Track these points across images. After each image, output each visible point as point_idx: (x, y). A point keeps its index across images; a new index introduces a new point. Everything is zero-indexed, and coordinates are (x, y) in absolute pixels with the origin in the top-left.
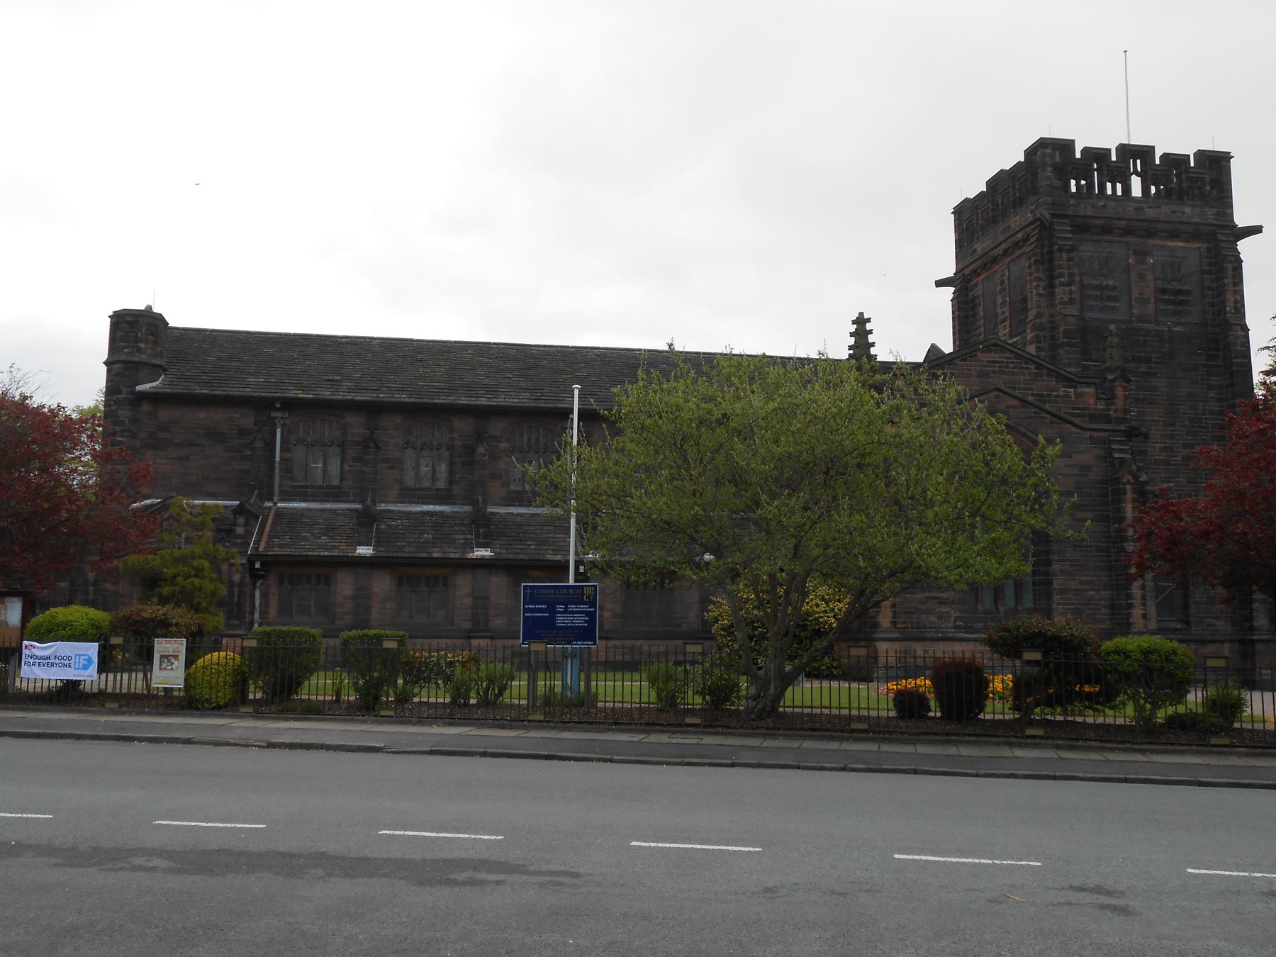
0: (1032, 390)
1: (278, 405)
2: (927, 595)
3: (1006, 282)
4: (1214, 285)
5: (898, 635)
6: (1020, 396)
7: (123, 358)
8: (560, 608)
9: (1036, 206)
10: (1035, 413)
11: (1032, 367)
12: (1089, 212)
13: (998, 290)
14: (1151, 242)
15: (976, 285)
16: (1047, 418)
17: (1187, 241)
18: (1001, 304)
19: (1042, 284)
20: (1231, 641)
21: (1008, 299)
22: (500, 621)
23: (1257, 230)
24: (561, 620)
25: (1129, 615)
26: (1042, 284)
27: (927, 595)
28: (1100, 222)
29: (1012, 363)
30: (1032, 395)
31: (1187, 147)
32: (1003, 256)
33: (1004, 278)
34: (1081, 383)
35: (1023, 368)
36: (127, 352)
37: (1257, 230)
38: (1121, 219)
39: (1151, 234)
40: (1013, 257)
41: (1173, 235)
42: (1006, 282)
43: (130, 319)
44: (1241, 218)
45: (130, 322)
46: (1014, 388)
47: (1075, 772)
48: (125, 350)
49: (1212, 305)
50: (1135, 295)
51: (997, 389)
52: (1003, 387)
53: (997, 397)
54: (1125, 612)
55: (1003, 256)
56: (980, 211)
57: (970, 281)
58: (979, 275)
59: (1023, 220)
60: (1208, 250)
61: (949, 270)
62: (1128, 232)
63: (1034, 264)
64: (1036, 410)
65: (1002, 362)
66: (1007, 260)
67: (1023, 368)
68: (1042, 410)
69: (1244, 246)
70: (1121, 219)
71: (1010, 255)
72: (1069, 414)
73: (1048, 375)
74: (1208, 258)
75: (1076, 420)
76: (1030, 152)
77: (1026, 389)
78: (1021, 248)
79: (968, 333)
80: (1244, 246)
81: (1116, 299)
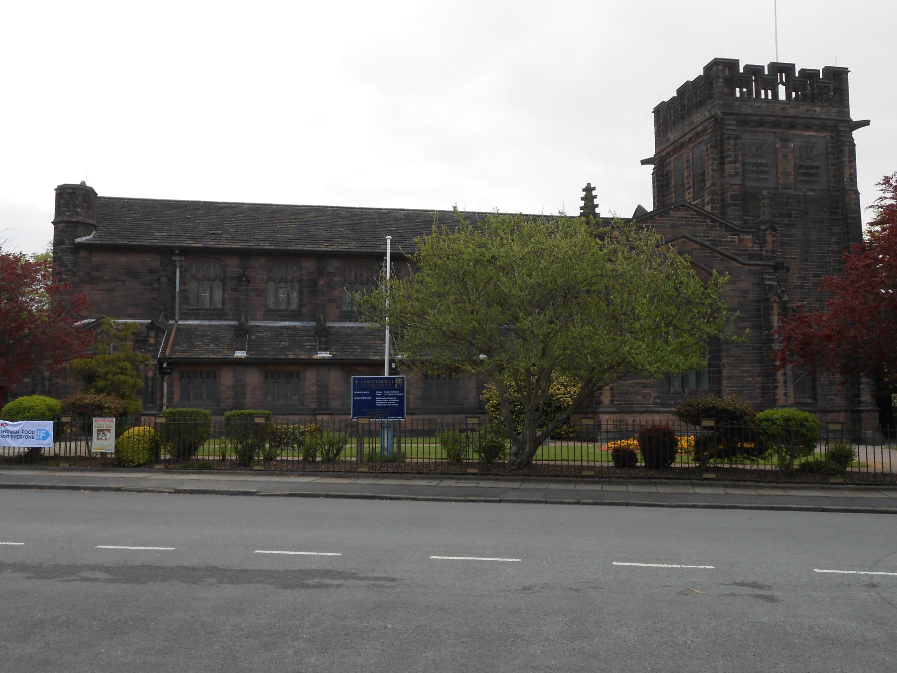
5: (615, 409)
6: (699, 241)
7: (65, 219)
8: (379, 393)
11: (709, 221)
12: (749, 111)
14: (792, 132)
15: (670, 163)
17: (816, 131)
19: (716, 162)
20: (845, 411)
23: (866, 123)
24: (379, 402)
25: (775, 394)
26: (716, 162)
29: (694, 218)
34: (742, 232)
37: (866, 123)
39: (792, 126)
40: (696, 143)
41: (808, 127)
44: (855, 115)
46: (696, 236)
50: (781, 169)
51: (684, 237)
52: (688, 235)
53: (684, 242)
60: (832, 137)
61: (651, 153)
62: (776, 125)
66: (691, 146)
67: (701, 222)
69: (856, 134)
72: (734, 254)
74: (831, 143)
75: (739, 259)
76: (707, 69)
77: (704, 237)
79: (664, 197)
80: (856, 134)
81: (767, 173)
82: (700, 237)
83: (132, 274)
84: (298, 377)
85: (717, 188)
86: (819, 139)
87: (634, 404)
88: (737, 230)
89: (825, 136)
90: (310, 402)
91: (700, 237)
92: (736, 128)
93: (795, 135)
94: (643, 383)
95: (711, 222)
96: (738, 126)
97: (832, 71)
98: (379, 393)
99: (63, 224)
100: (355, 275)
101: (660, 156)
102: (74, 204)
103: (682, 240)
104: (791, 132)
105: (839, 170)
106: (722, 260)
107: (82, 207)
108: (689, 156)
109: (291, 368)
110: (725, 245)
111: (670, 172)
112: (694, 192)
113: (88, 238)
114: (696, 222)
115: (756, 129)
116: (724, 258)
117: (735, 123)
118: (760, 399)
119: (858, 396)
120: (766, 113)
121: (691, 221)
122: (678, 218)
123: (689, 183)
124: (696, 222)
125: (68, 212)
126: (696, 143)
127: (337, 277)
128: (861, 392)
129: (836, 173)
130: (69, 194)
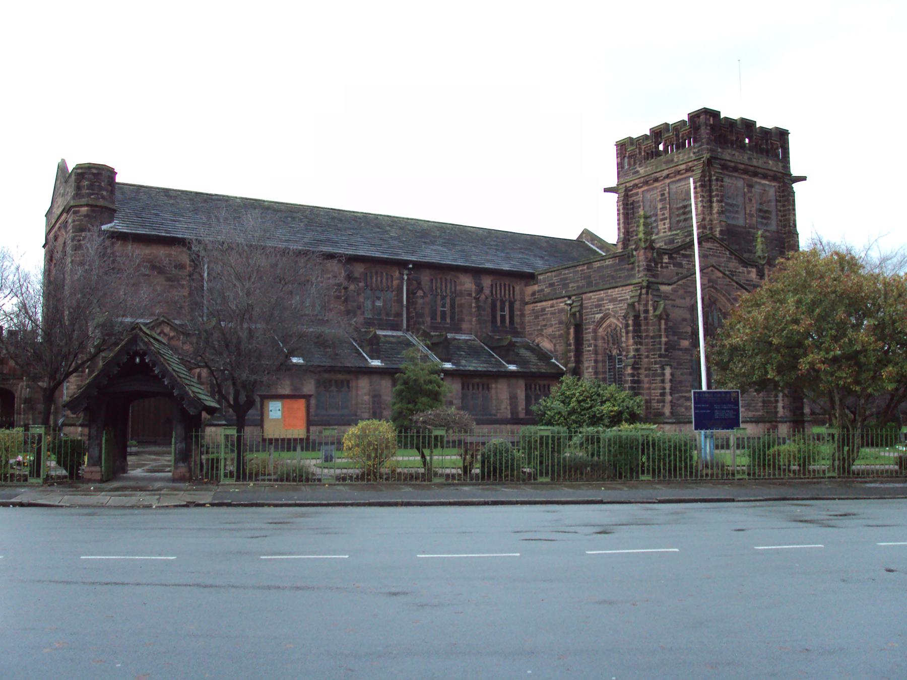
0: (728, 267)
1: (411, 266)
2: (680, 395)
3: (667, 195)
4: (782, 209)
7: (90, 202)
8: (716, 406)
9: (699, 150)
10: (730, 282)
12: (728, 158)
13: (658, 199)
16: (734, 286)
17: (770, 181)
18: (660, 209)
20: (790, 422)
21: (668, 206)
22: (387, 413)
23: (803, 179)
27: (680, 395)
28: (732, 164)
29: (719, 250)
30: (729, 271)
31: (769, 125)
32: (665, 178)
33: (665, 192)
34: (749, 265)
35: (723, 254)
36: (93, 198)
37: (803, 179)
38: (741, 164)
39: (755, 174)
40: (674, 179)
41: (765, 177)
42: (667, 195)
43: (94, 171)
44: (795, 171)
45: (95, 174)
47: (302, 500)
48: (92, 197)
49: (781, 221)
50: (748, 212)
51: (713, 266)
53: (712, 271)
54: (774, 405)
55: (665, 178)
56: (643, 147)
57: (631, 190)
58: (640, 187)
59: (686, 157)
60: (779, 187)
61: (613, 182)
62: (745, 172)
63: (700, 187)
64: (730, 280)
65: (714, 249)
66: (667, 181)
67: (723, 254)
68: (733, 280)
69: (796, 186)
70: (741, 164)
71: (671, 178)
72: (744, 283)
73: (735, 259)
74: (779, 192)
77: (725, 267)
78: (682, 174)
79: (628, 224)
80: (796, 186)
81: (737, 212)
82: (722, 267)
83: (157, 268)
84: (348, 387)
85: (706, 222)
86: (771, 188)
87: (679, 416)
88: (746, 263)
89: (774, 186)
90: (362, 412)
91: (722, 267)
92: (721, 171)
93: (756, 182)
94: (685, 397)
95: (730, 254)
96: (722, 169)
97: (780, 131)
98: (716, 406)
99: (86, 208)
100: (377, 281)
101: (626, 186)
102: (100, 186)
103: (711, 268)
104: (753, 179)
105: (784, 216)
106: (737, 288)
107: (107, 190)
108: (665, 190)
109: (340, 377)
110: (739, 276)
111: (638, 202)
112: (670, 223)
113: (109, 225)
114: (720, 253)
115: (731, 174)
116: (738, 287)
117: (720, 167)
118: (762, 411)
119: (802, 408)
120: (739, 161)
121: (717, 253)
122: (708, 248)
123: (663, 214)
124: (720, 253)
125: (93, 194)
126: (674, 179)
127: (361, 282)
128: (804, 405)
129: (782, 218)
130: (94, 174)
